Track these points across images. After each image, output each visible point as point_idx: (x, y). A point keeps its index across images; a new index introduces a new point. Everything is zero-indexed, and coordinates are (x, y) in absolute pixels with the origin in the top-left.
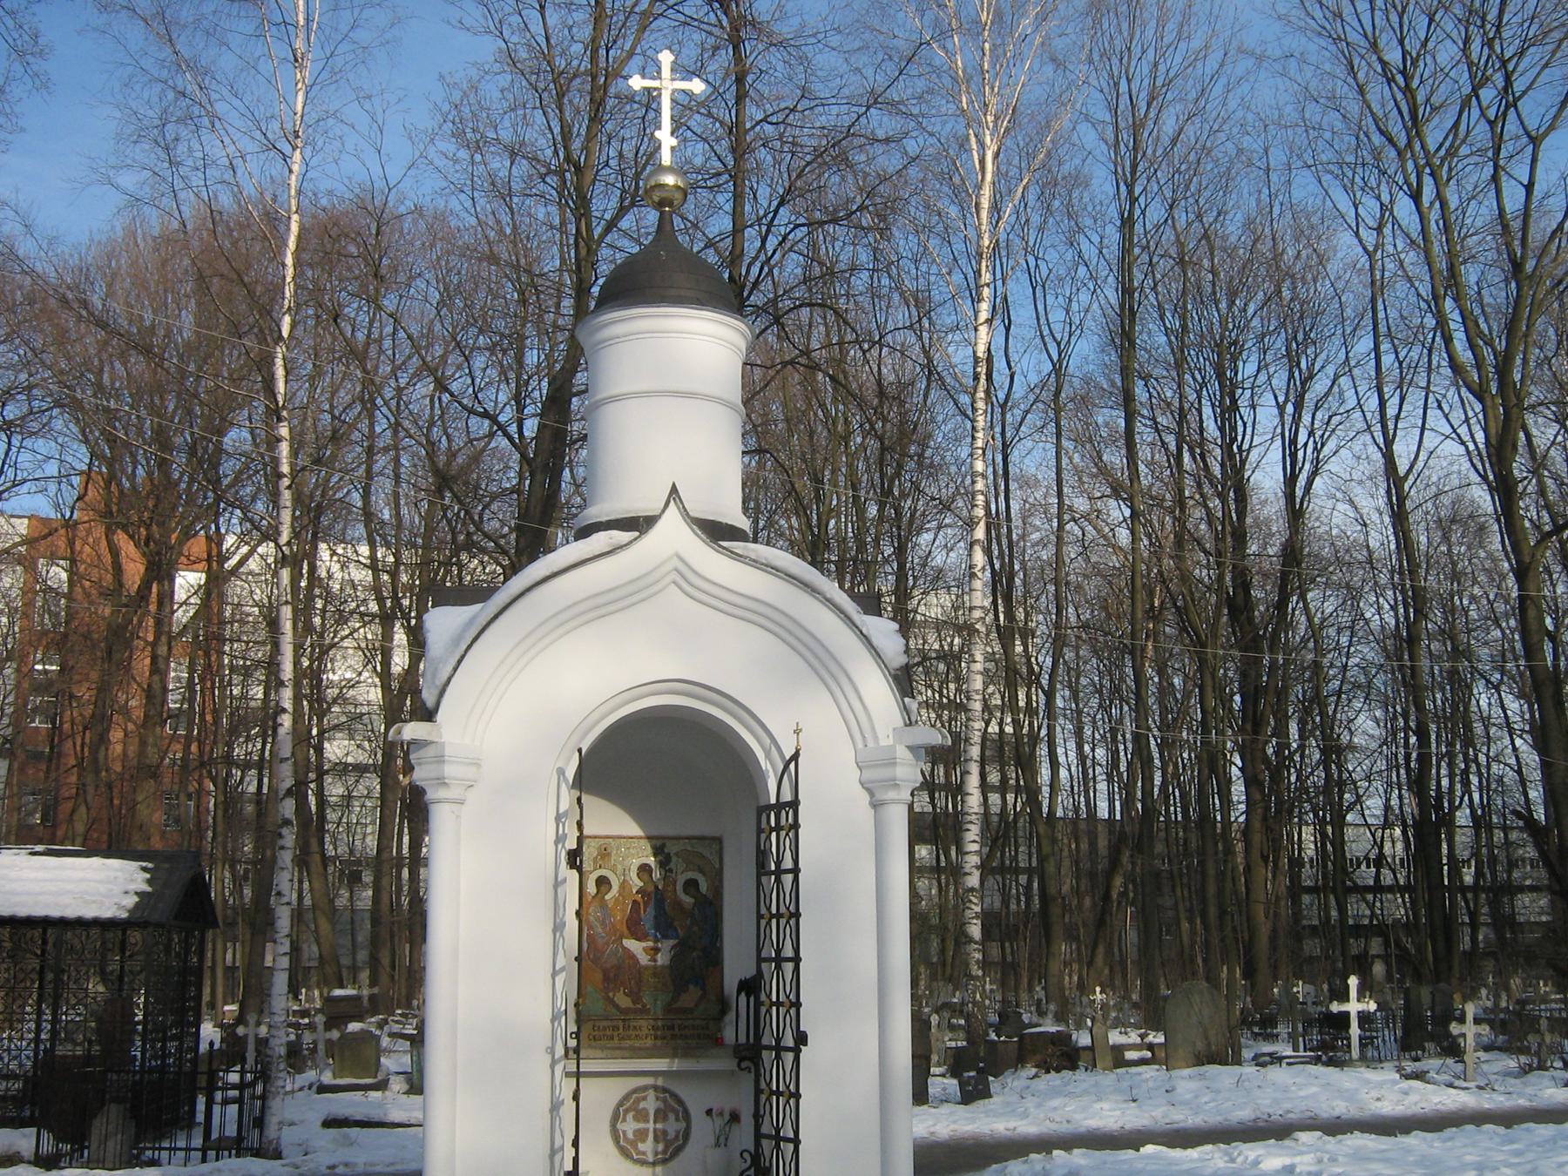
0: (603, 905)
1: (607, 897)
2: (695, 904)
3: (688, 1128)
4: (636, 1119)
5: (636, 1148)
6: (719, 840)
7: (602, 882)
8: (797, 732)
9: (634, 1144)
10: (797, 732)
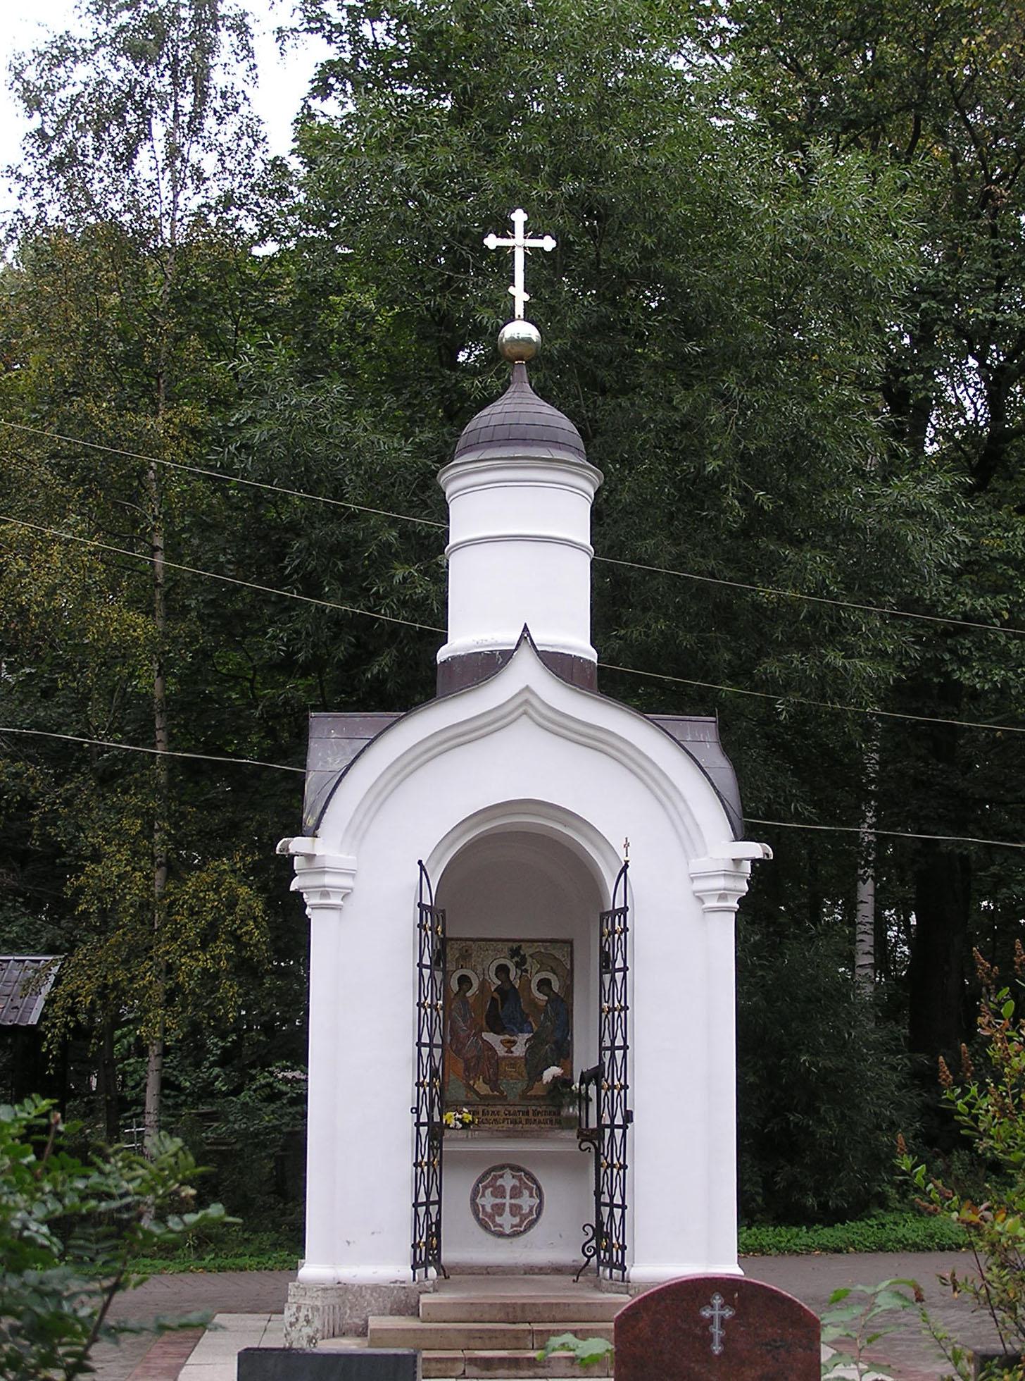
0: (465, 1001)
1: (468, 994)
2: (547, 1002)
3: (541, 1204)
4: (494, 1195)
5: (493, 1221)
6: (570, 943)
7: (464, 980)
8: (627, 846)
9: (491, 1217)
10: (627, 846)
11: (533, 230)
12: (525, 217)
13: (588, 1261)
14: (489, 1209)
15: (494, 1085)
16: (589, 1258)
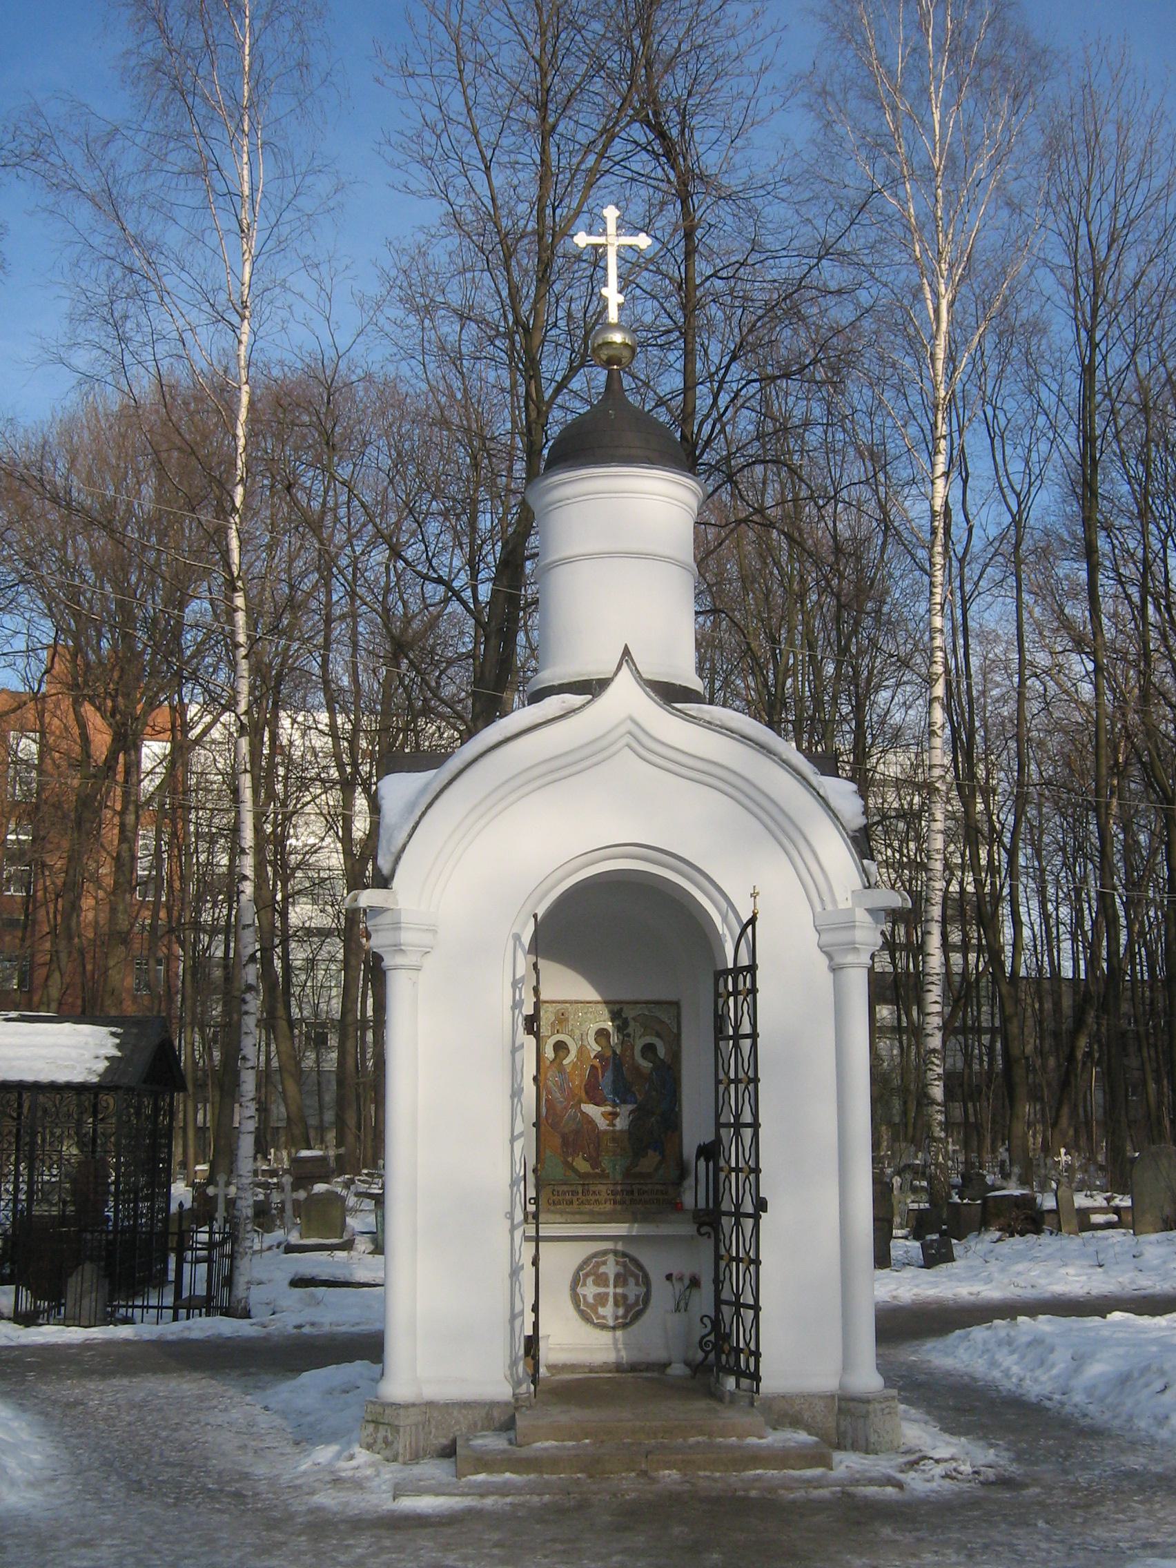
0: (561, 1069)
1: (565, 1062)
4: (596, 1283)
5: (596, 1313)
6: (676, 1004)
7: (560, 1047)
11: (626, 226)
12: (617, 213)
13: (706, 1358)
14: (591, 1300)
15: (595, 1163)
16: (707, 1353)
